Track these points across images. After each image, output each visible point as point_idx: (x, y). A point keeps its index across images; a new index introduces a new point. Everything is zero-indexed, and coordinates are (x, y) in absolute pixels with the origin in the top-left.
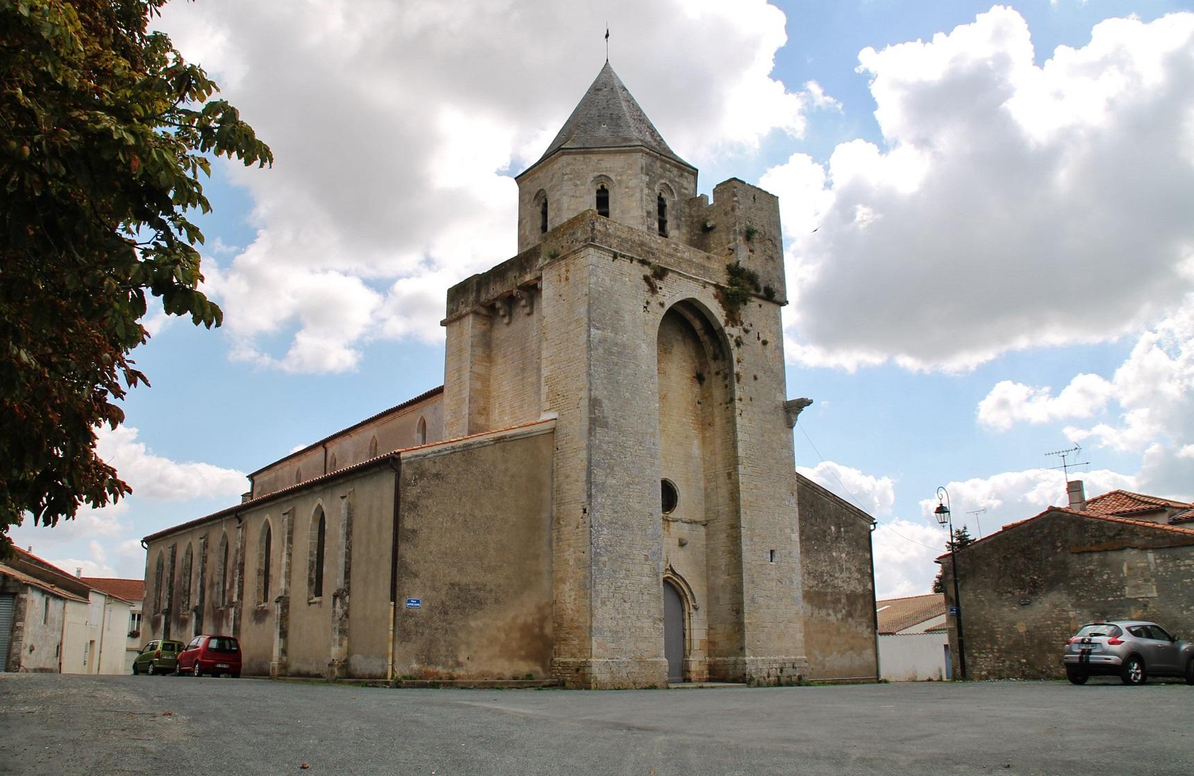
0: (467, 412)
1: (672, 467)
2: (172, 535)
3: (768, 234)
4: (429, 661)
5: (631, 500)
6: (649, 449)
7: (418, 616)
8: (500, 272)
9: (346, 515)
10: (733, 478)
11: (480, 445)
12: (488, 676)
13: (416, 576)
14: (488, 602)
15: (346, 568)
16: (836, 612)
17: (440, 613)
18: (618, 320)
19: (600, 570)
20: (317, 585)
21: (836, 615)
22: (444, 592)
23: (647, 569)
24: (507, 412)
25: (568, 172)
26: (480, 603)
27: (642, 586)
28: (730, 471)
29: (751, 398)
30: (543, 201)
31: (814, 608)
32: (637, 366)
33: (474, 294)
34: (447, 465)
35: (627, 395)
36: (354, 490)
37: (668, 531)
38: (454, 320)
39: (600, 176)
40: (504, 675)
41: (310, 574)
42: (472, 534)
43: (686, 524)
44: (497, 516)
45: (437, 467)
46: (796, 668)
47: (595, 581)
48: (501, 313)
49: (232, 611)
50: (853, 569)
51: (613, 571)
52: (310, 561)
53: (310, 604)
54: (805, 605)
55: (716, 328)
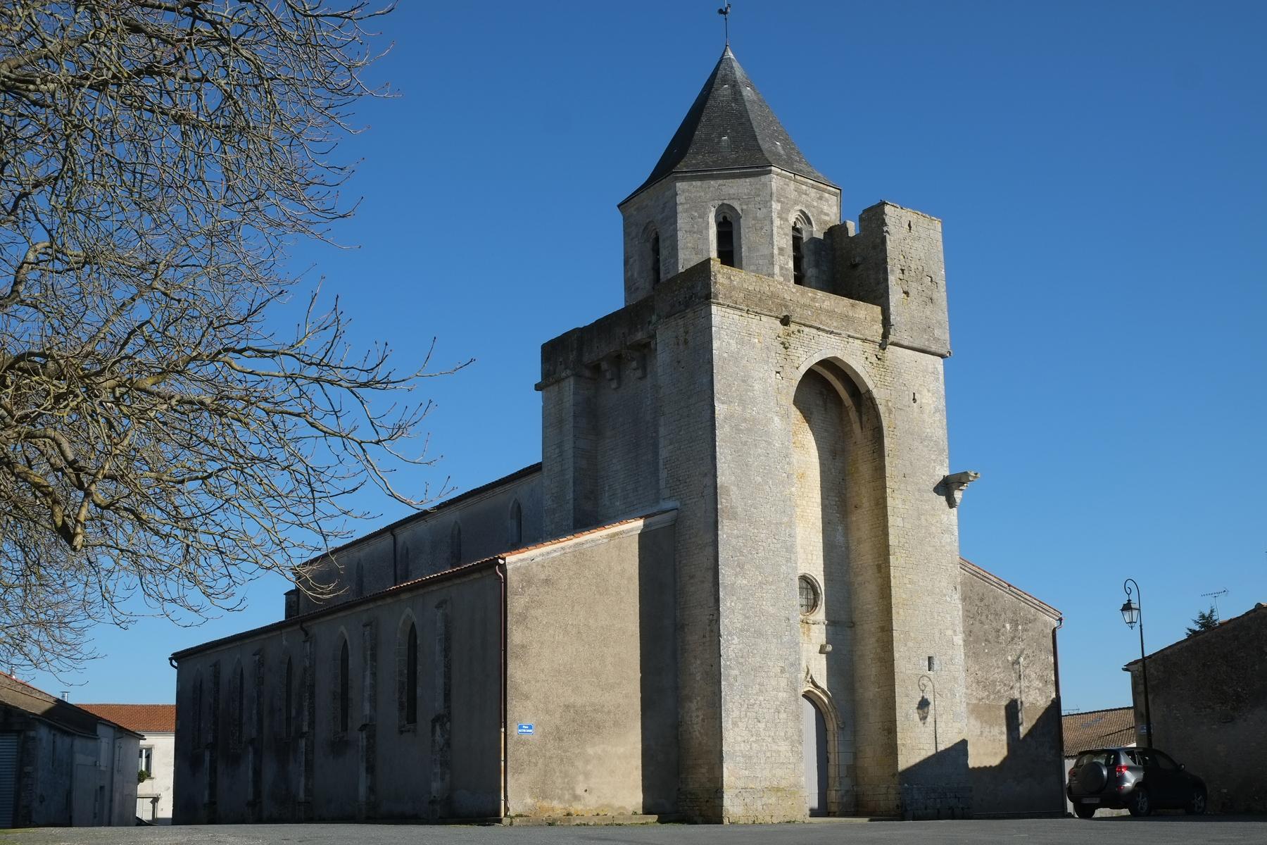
0: (571, 496)
1: (812, 560)
3: (926, 269)
4: (544, 795)
5: (764, 603)
6: (785, 542)
8: (605, 325)
9: (443, 628)
10: (883, 570)
13: (527, 697)
14: (607, 725)
17: (554, 739)
18: (747, 391)
20: (410, 708)
23: (783, 683)
24: (619, 495)
28: (880, 562)
30: (653, 235)
32: (769, 443)
33: (574, 353)
35: (759, 479)
36: (1070, 816)
42: (587, 646)
48: (608, 376)
49: (303, 743)
50: (1033, 676)
51: (745, 686)
52: (400, 681)
53: (401, 732)
54: (973, 721)
55: (863, 391)
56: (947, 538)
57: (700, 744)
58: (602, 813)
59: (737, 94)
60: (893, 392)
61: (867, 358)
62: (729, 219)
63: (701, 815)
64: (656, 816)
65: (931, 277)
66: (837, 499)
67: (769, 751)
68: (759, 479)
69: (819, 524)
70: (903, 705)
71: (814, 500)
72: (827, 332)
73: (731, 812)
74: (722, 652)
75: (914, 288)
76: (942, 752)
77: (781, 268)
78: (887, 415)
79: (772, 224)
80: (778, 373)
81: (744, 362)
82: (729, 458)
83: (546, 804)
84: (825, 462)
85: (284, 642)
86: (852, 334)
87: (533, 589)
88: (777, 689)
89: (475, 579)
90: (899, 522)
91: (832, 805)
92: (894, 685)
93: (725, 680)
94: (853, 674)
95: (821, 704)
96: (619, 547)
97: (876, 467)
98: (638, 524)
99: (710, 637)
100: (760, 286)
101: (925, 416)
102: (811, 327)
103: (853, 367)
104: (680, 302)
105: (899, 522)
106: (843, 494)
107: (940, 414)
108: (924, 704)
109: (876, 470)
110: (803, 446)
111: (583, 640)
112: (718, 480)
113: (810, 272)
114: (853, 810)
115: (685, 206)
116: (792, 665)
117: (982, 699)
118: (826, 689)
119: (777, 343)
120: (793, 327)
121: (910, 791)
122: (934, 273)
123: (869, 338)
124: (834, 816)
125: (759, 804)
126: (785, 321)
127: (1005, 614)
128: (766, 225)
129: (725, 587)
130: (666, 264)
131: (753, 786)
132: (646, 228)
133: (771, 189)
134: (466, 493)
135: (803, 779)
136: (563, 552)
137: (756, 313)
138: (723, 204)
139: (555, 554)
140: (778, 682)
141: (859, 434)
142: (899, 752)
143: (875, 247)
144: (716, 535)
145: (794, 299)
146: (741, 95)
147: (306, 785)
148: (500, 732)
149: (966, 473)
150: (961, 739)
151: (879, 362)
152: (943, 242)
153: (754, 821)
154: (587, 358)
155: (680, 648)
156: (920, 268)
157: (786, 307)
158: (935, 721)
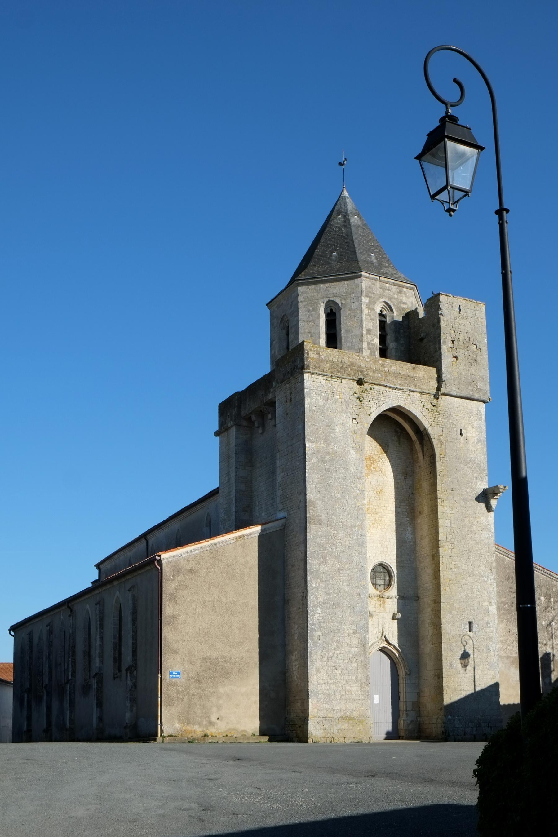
0: (234, 510)
1: (387, 552)
2: (29, 624)
3: (472, 339)
4: (188, 722)
5: (341, 583)
7: (179, 685)
9: (132, 605)
11: (224, 544)
13: (176, 652)
14: (233, 671)
15: (133, 648)
17: (196, 682)
18: (330, 432)
22: (198, 665)
23: (355, 641)
27: (351, 656)
28: (434, 553)
32: (347, 469)
33: (236, 409)
34: (198, 561)
35: (338, 495)
37: (383, 607)
38: (224, 431)
41: (114, 654)
42: (219, 616)
45: (191, 565)
48: (256, 424)
52: (114, 642)
53: (115, 678)
55: (422, 429)
56: (485, 534)
57: (297, 685)
58: (229, 735)
59: (346, 222)
60: (444, 430)
61: (424, 406)
62: (334, 311)
63: (297, 737)
64: (268, 737)
65: (476, 345)
66: (407, 508)
68: (338, 495)
69: (393, 526)
70: (448, 657)
72: (393, 388)
73: (314, 735)
74: (309, 619)
75: (462, 354)
76: (478, 691)
77: (369, 344)
78: (439, 446)
79: (362, 312)
80: (355, 419)
81: (329, 412)
82: (316, 480)
83: (189, 728)
84: (399, 481)
85: (62, 617)
86: (412, 389)
87: (181, 577)
88: (350, 646)
89: (148, 570)
90: (447, 523)
91: (401, 730)
92: (441, 643)
93: (311, 639)
94: (418, 635)
95: (394, 657)
96: (243, 546)
97: (432, 483)
98: (256, 529)
99: (303, 608)
100: (342, 358)
101: (470, 446)
102: (380, 385)
103: (413, 412)
104: (288, 372)
105: (447, 523)
106: (412, 503)
107: (482, 444)
108: (465, 656)
109: (432, 485)
110: (381, 470)
111: (216, 612)
112: (307, 497)
113: (391, 345)
114: (416, 735)
115: (304, 304)
116: (361, 628)
118: (397, 646)
119: (354, 398)
120: (367, 386)
121: (452, 721)
122: (479, 342)
123: (425, 391)
124: (402, 739)
125: (335, 729)
126: (360, 382)
127: (541, 589)
128: (358, 314)
129: (312, 573)
130: (292, 344)
131: (331, 716)
132: (282, 320)
133: (362, 288)
134: (182, 509)
135: (369, 711)
136: (202, 550)
137: (338, 377)
138: (329, 301)
139: (196, 552)
141: (422, 460)
142: (444, 692)
143: (434, 326)
144: (306, 536)
145: (368, 366)
146: (349, 222)
147: (70, 716)
148: (158, 677)
149: (497, 486)
150: (495, 682)
151: (434, 408)
152: (486, 319)
153: (331, 741)
154: (243, 413)
155: (286, 617)
156: (468, 339)
157: (362, 372)
158: (474, 668)
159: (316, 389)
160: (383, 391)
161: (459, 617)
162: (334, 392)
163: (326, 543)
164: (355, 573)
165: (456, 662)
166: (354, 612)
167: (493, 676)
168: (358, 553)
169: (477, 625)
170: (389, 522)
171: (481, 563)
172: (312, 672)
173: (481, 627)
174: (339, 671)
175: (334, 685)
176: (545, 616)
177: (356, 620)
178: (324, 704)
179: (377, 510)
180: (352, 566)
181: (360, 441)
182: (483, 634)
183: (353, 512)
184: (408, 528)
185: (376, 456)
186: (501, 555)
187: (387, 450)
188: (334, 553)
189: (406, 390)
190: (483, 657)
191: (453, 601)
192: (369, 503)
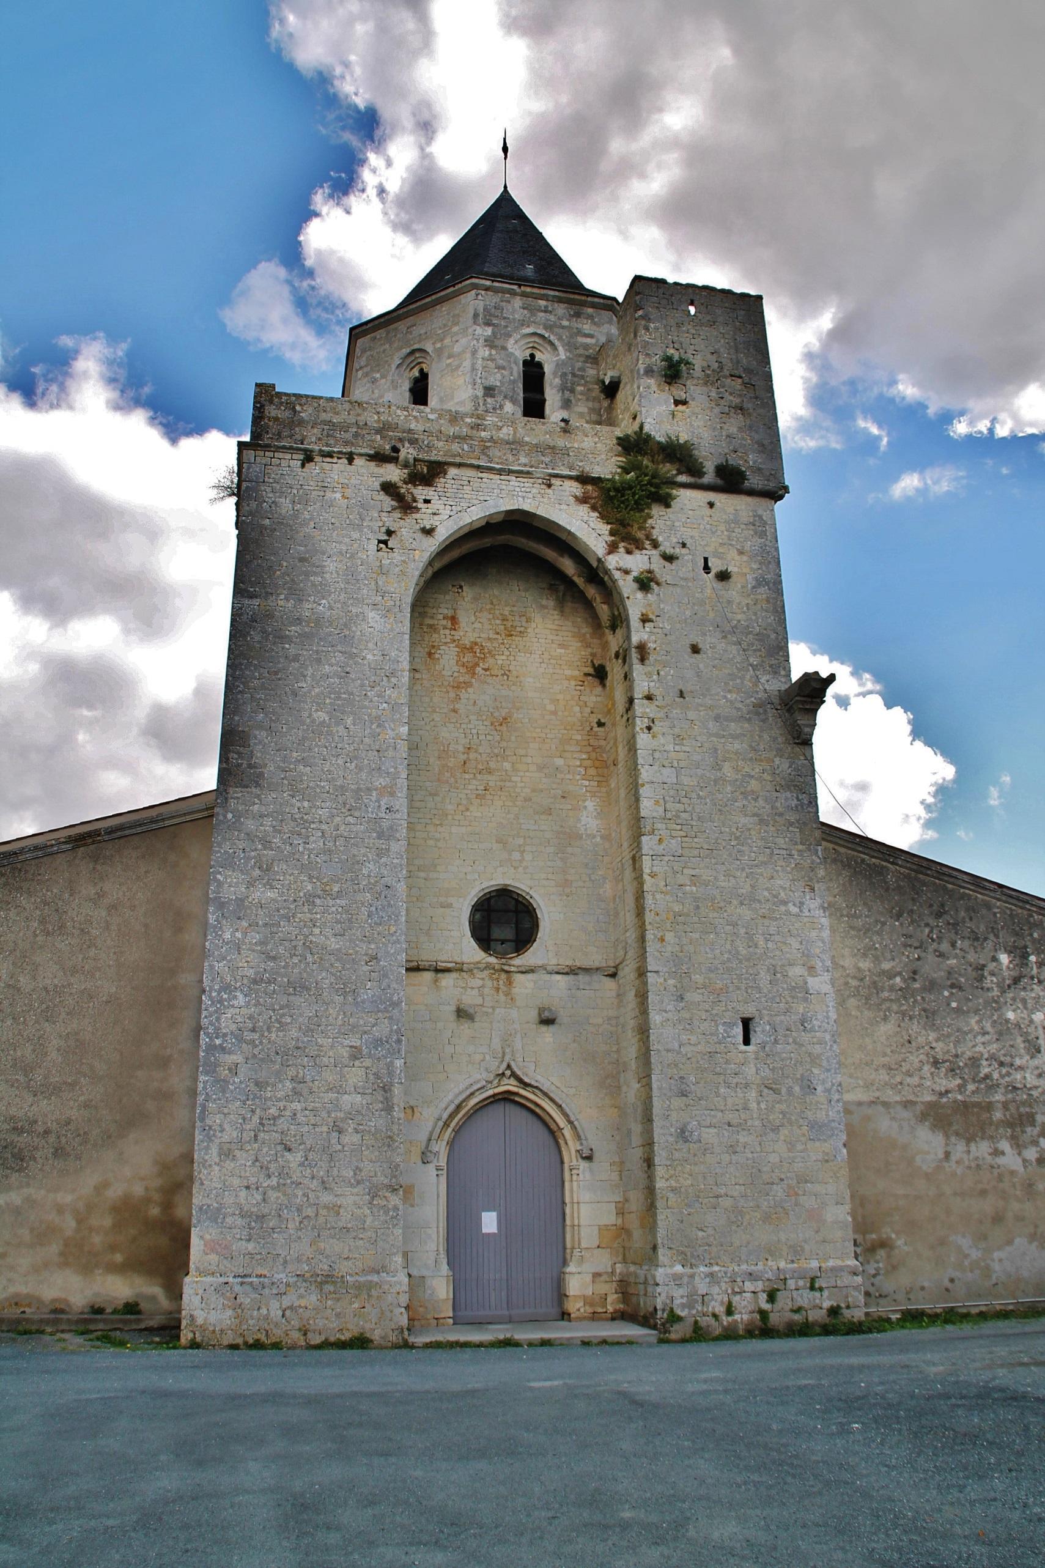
12: (29, 1305)
14: (38, 1155)
16: (1018, 1146)
19: (222, 1084)
21: (1019, 1154)
23: (355, 1076)
25: (362, 364)
26: (20, 1157)
27: (341, 1115)
29: (681, 692)
31: (953, 1139)
32: (352, 656)
35: (322, 716)
39: (413, 352)
40: (69, 1305)
43: (559, 977)
44: (70, 985)
46: (821, 1289)
47: (204, 1108)
51: (257, 1084)
67: (310, 1205)
71: (529, 760)
72: (500, 472)
107: (769, 589)
117: (947, 1092)
125: (274, 1309)
140: (342, 1076)
159: (275, 482)
160: (472, 479)
161: (707, 1007)
162: (326, 485)
163: (275, 831)
164: (363, 904)
165: (699, 1124)
166: (356, 1004)
167: (827, 1154)
168: (377, 855)
169: (768, 1027)
170: (527, 790)
171: (777, 871)
172: (207, 1157)
173: (781, 1032)
174: (299, 1155)
175: (279, 1191)
176: (1014, 999)
177: (361, 1022)
178: (244, 1242)
179: (492, 765)
180: (356, 887)
181: (397, 591)
182: (789, 1047)
183: (366, 756)
184: (587, 804)
185: (492, 643)
186: (873, 860)
187: (526, 628)
188: (297, 856)
189: (538, 476)
190: (792, 1107)
191: (688, 969)
192: (469, 748)
